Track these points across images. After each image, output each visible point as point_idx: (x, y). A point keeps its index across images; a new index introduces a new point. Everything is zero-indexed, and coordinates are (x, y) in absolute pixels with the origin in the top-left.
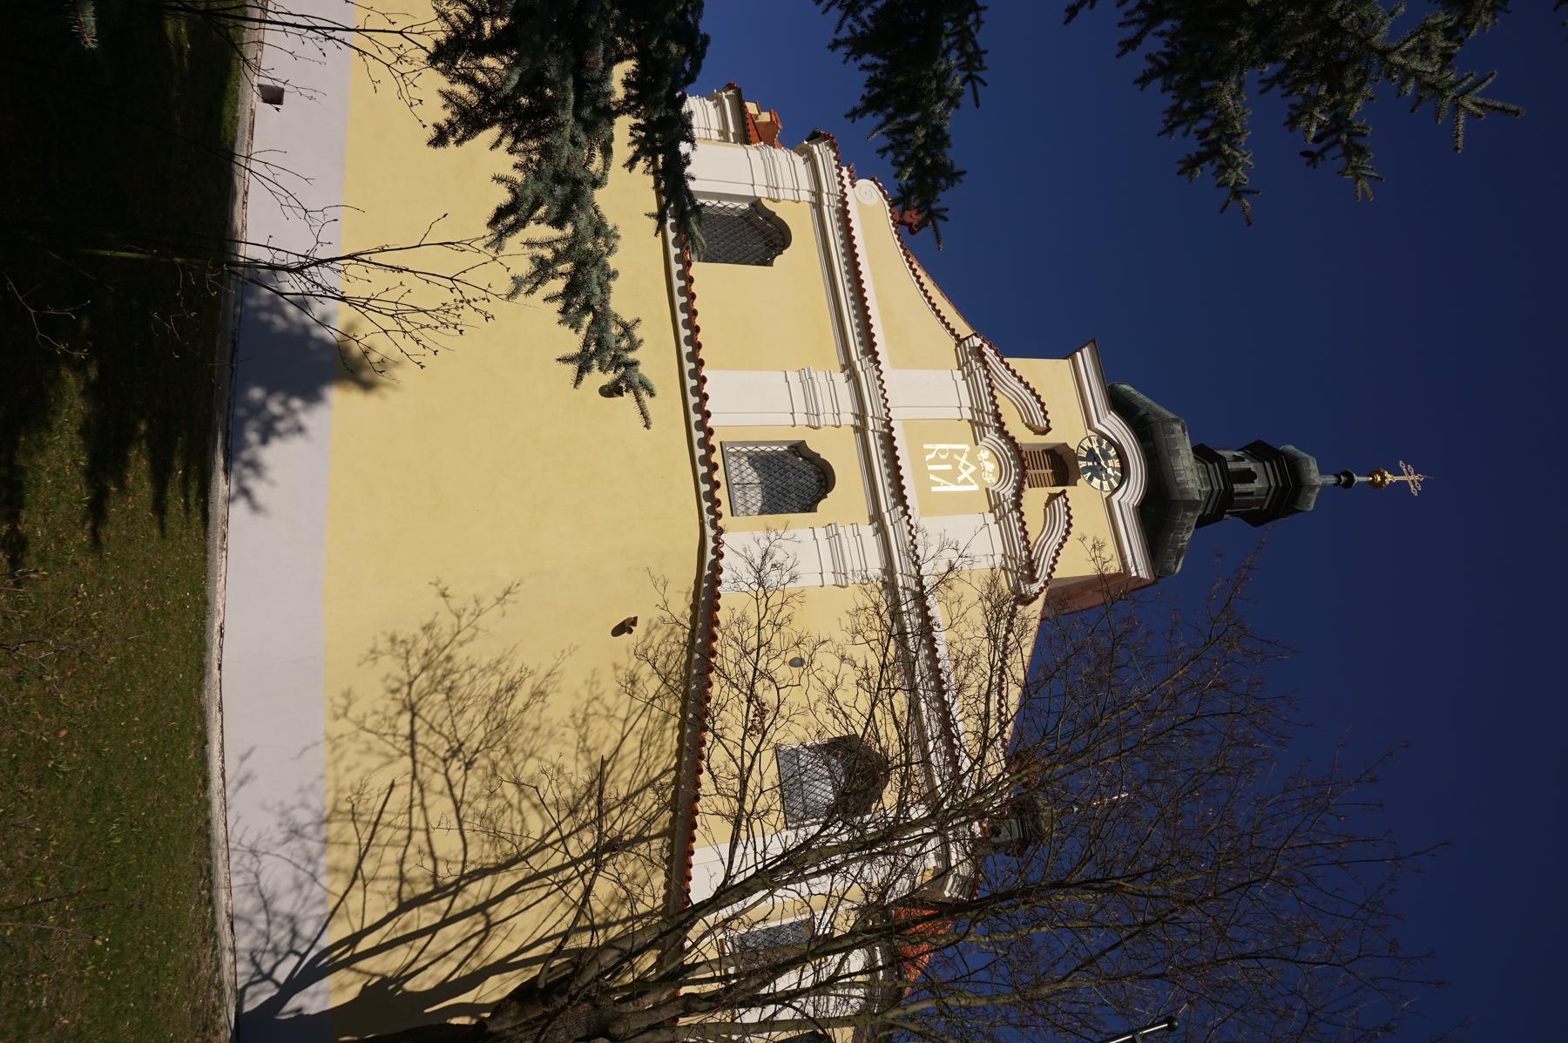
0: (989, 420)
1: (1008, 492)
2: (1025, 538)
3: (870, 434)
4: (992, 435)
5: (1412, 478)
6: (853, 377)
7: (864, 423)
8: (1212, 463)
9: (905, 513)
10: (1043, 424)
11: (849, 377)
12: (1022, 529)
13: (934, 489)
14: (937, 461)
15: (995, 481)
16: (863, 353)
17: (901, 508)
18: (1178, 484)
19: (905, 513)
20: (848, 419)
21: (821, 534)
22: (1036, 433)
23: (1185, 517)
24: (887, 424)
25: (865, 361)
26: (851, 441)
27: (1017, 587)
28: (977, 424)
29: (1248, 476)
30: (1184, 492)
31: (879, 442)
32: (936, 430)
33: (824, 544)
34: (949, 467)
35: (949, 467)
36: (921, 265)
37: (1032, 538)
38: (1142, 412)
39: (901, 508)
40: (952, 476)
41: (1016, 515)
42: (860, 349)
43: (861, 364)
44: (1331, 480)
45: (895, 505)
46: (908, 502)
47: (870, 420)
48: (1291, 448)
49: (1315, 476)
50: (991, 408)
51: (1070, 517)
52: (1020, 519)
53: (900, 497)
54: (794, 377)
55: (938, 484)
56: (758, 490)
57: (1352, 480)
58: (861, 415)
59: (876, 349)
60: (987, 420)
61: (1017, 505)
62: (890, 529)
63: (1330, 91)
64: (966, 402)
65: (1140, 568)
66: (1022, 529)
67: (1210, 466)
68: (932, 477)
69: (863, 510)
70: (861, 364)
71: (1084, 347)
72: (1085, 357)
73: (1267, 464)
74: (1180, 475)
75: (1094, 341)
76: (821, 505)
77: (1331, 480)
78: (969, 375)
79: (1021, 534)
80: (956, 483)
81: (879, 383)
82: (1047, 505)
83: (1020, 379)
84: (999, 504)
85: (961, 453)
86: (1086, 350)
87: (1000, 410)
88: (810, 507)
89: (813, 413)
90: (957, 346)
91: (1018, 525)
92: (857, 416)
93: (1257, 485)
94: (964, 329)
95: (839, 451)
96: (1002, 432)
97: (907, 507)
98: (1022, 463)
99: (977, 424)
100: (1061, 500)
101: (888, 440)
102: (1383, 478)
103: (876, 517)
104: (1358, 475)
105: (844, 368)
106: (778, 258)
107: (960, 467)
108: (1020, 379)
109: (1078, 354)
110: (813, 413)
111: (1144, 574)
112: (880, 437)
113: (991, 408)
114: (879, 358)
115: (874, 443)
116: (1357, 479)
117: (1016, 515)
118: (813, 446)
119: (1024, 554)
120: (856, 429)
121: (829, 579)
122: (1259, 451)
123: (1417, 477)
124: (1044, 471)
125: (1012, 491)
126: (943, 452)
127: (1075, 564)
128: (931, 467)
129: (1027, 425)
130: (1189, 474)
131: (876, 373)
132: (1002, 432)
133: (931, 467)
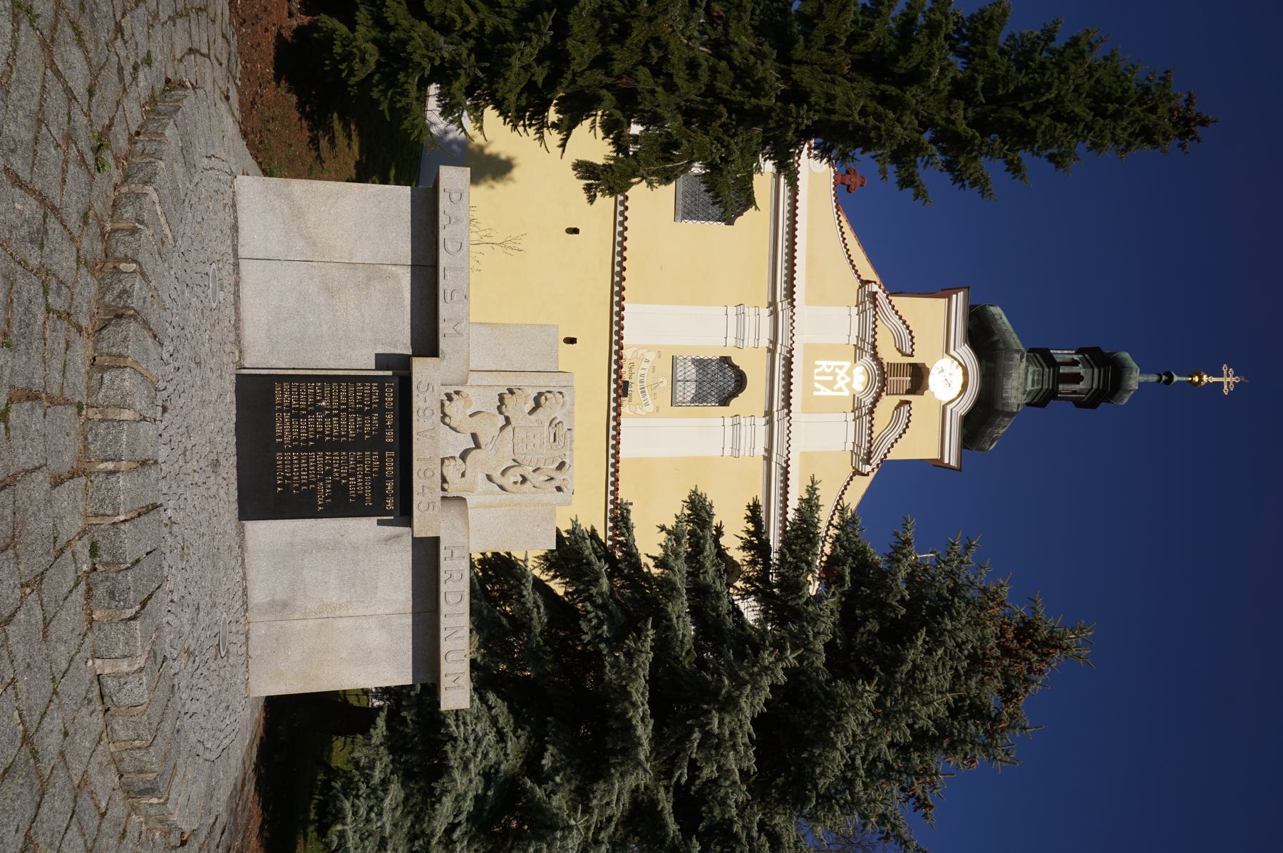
0: (868, 347)
1: (868, 400)
2: (870, 435)
3: (777, 355)
4: (867, 358)
5: (1228, 380)
6: (774, 313)
7: (775, 347)
8: (1049, 367)
9: (788, 414)
10: (909, 351)
11: (772, 313)
12: (870, 428)
13: (816, 393)
14: (823, 373)
15: (862, 389)
16: (785, 296)
17: (786, 411)
18: (1003, 399)
19: (788, 414)
20: (765, 343)
21: (728, 421)
22: (904, 354)
23: (1002, 420)
24: (790, 351)
25: (785, 303)
26: (764, 358)
27: (1083, 120)
28: (859, 348)
29: (1077, 378)
30: (1007, 405)
31: (782, 362)
32: (830, 352)
33: (729, 430)
34: (831, 378)
35: (831, 378)
36: (850, 220)
37: (874, 436)
38: (996, 338)
39: (786, 411)
40: (830, 385)
41: (869, 418)
42: (784, 292)
43: (782, 305)
44: (1154, 378)
45: (783, 408)
46: (792, 408)
47: (779, 346)
48: (1126, 355)
49: (1135, 379)
50: (871, 340)
51: (909, 421)
52: (870, 422)
53: (787, 403)
54: (732, 311)
55: (819, 390)
56: (694, 386)
57: (1171, 377)
58: (774, 342)
59: (795, 296)
60: (867, 347)
61: (871, 412)
62: (776, 423)
63: (637, 797)
64: (855, 333)
65: (951, 459)
66: (870, 428)
67: (1046, 370)
68: (817, 385)
69: (762, 407)
70: (782, 305)
71: (956, 290)
72: (959, 299)
73: (1096, 370)
74: (1007, 392)
75: (969, 288)
76: (734, 402)
77: (1154, 378)
78: (862, 312)
79: (869, 432)
80: (833, 390)
81: (791, 321)
82: (896, 408)
83: (900, 318)
84: (860, 408)
85: (841, 368)
86: (961, 294)
87: (876, 343)
88: (724, 402)
89: (740, 338)
90: (860, 287)
91: (868, 425)
92: (771, 342)
93: (1081, 386)
94: (868, 272)
95: (754, 367)
96: (875, 356)
97: (790, 411)
98: (883, 376)
99: (859, 348)
100: (907, 407)
101: (788, 362)
102: (1201, 380)
103: (769, 413)
104: (1178, 375)
105: (770, 305)
106: (739, 219)
107: (838, 378)
108: (900, 318)
109: (954, 296)
110: (740, 338)
111: (953, 463)
112: (784, 359)
113: (871, 340)
114: (795, 303)
115: (779, 362)
116: (1176, 378)
117: (869, 418)
118: (735, 361)
119: (867, 445)
120: (769, 350)
121: (728, 452)
122: (1096, 357)
123: (1234, 379)
124: (905, 378)
125: (871, 400)
126: (829, 367)
127: (906, 450)
128: (816, 378)
129: (898, 349)
130: (1014, 392)
131: (791, 314)
132: (875, 356)
133: (816, 378)
